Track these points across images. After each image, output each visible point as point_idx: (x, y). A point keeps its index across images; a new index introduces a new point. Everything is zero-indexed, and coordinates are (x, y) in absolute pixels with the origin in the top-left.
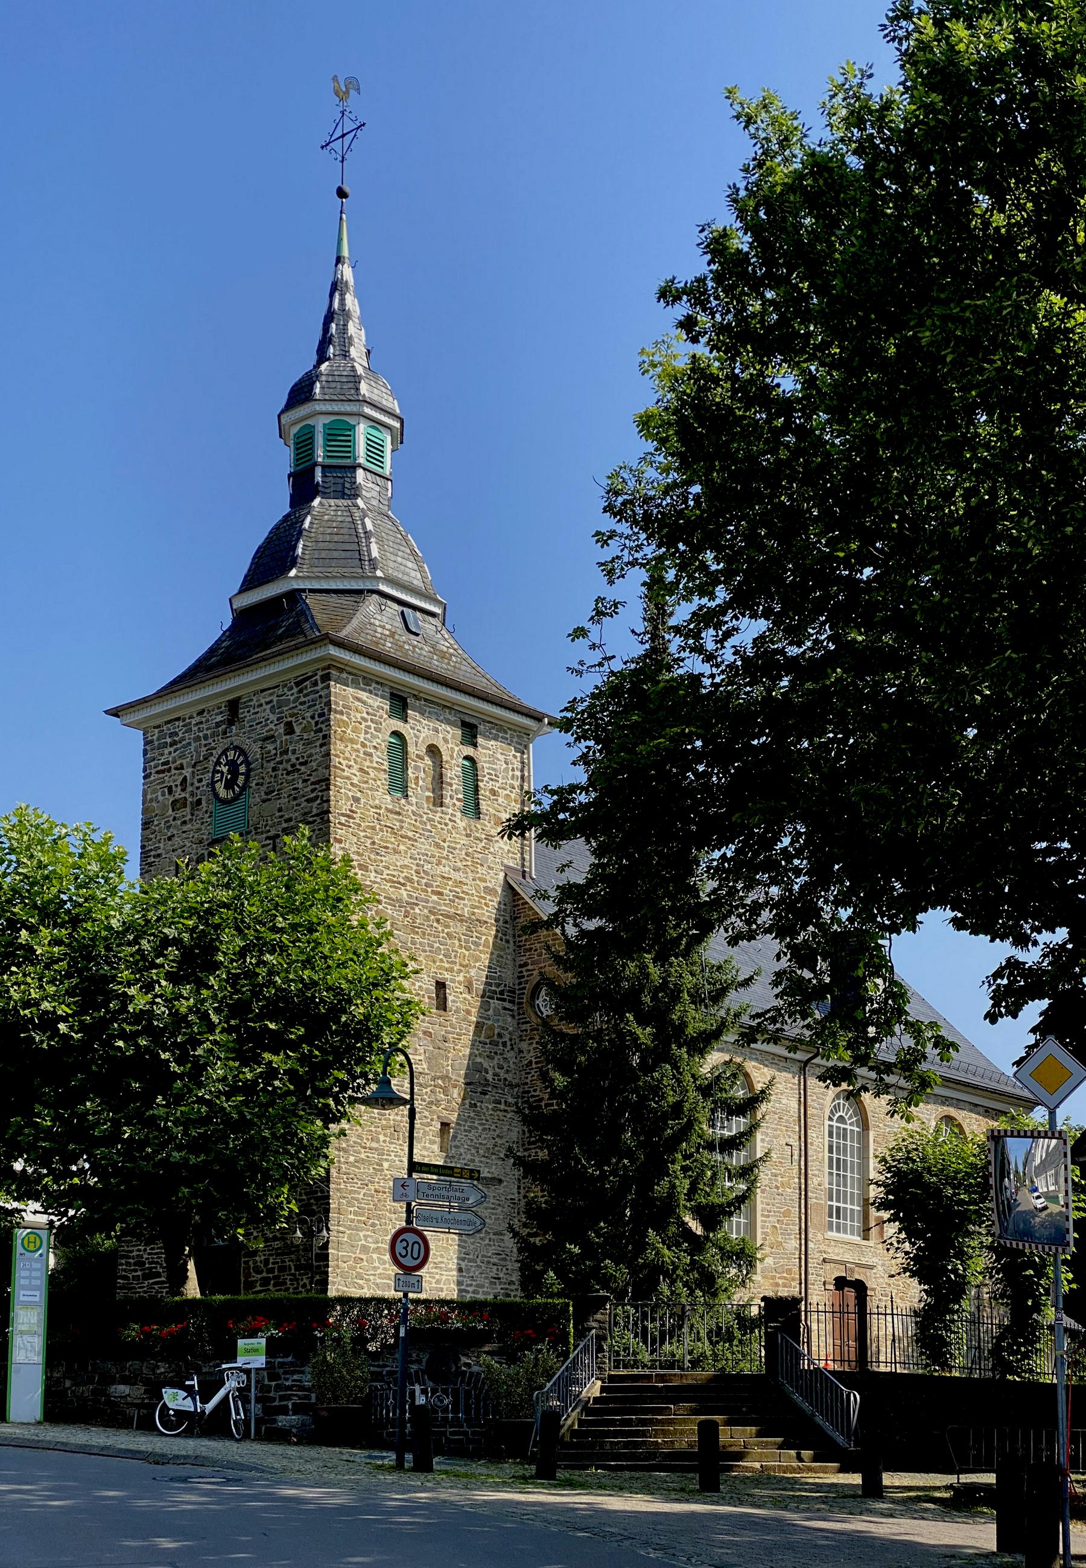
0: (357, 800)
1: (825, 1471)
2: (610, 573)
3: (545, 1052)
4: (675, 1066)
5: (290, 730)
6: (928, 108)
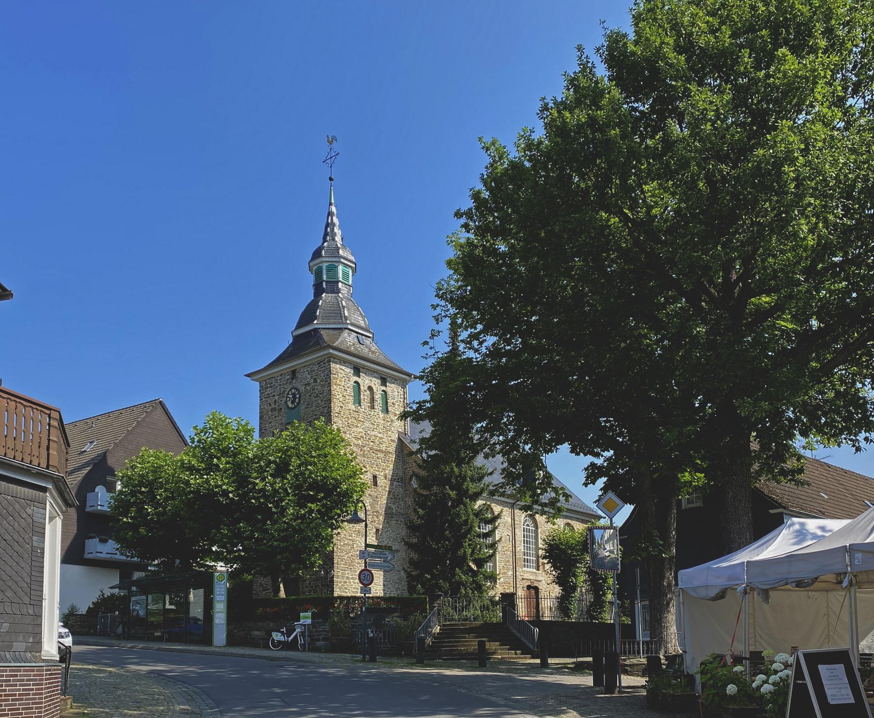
0: (342, 407)
1: (525, 658)
2: (437, 320)
3: (415, 501)
4: (465, 506)
5: (315, 381)
6: (556, 144)
